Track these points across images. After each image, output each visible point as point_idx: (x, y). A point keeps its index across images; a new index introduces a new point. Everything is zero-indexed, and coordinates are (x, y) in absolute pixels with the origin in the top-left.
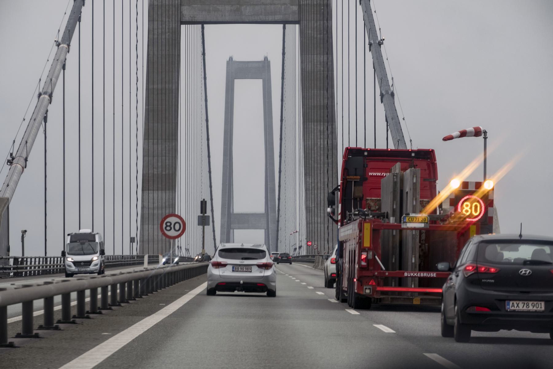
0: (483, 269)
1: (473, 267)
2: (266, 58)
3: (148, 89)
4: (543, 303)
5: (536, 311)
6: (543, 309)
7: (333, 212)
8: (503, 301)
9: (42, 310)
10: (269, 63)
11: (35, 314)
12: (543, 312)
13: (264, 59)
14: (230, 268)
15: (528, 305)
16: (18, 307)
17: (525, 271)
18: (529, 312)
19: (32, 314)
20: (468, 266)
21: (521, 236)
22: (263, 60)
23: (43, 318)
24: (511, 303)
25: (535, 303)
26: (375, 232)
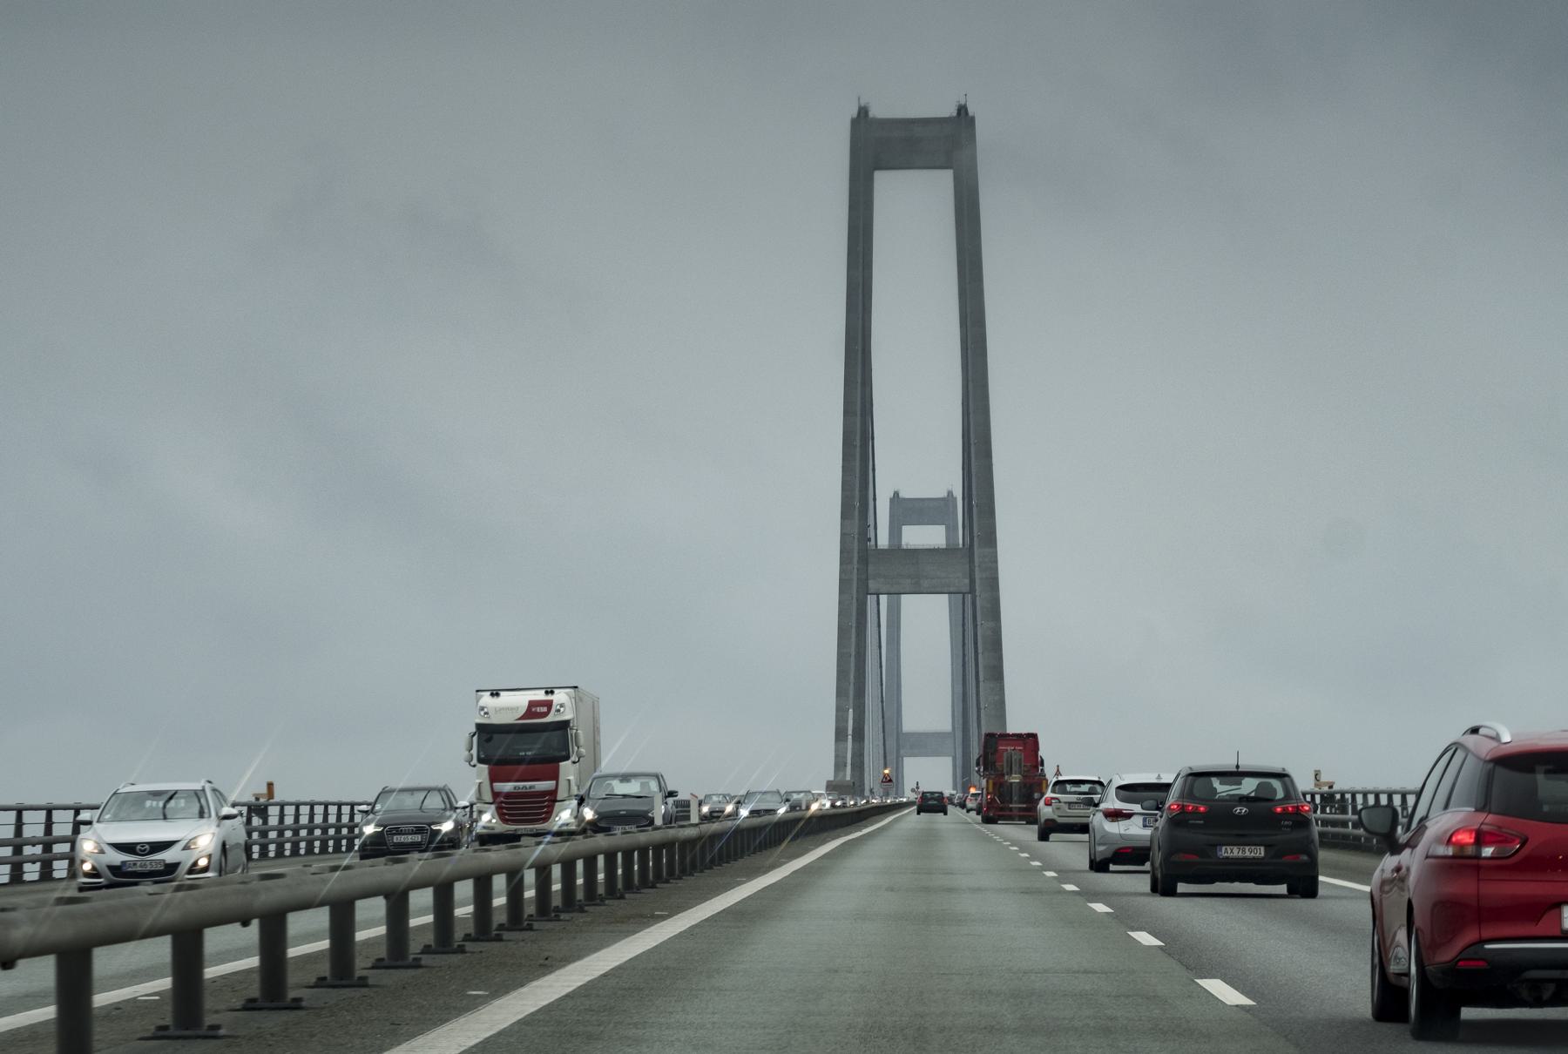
0: (1190, 808)
1: (1178, 806)
2: (962, 110)
3: (864, 678)
4: (1262, 848)
5: (1254, 858)
6: (1263, 854)
7: (979, 770)
8: (1215, 846)
9: (163, 977)
10: (971, 121)
11: (414, 922)
12: (1263, 858)
13: (956, 112)
14: (1138, 820)
15: (1244, 851)
16: (320, 918)
17: (1241, 810)
18: (1245, 858)
19: (284, 952)
20: (1172, 805)
21: (1238, 767)
22: (955, 114)
23: (256, 977)
24: (1224, 848)
25: (1253, 848)
26: (994, 784)
